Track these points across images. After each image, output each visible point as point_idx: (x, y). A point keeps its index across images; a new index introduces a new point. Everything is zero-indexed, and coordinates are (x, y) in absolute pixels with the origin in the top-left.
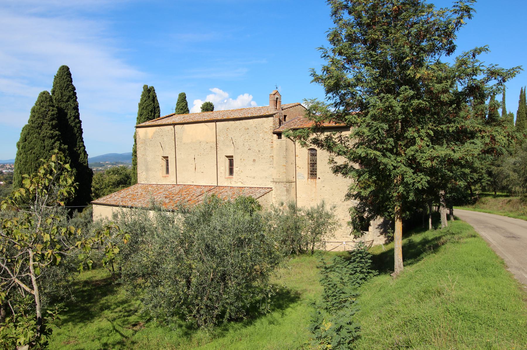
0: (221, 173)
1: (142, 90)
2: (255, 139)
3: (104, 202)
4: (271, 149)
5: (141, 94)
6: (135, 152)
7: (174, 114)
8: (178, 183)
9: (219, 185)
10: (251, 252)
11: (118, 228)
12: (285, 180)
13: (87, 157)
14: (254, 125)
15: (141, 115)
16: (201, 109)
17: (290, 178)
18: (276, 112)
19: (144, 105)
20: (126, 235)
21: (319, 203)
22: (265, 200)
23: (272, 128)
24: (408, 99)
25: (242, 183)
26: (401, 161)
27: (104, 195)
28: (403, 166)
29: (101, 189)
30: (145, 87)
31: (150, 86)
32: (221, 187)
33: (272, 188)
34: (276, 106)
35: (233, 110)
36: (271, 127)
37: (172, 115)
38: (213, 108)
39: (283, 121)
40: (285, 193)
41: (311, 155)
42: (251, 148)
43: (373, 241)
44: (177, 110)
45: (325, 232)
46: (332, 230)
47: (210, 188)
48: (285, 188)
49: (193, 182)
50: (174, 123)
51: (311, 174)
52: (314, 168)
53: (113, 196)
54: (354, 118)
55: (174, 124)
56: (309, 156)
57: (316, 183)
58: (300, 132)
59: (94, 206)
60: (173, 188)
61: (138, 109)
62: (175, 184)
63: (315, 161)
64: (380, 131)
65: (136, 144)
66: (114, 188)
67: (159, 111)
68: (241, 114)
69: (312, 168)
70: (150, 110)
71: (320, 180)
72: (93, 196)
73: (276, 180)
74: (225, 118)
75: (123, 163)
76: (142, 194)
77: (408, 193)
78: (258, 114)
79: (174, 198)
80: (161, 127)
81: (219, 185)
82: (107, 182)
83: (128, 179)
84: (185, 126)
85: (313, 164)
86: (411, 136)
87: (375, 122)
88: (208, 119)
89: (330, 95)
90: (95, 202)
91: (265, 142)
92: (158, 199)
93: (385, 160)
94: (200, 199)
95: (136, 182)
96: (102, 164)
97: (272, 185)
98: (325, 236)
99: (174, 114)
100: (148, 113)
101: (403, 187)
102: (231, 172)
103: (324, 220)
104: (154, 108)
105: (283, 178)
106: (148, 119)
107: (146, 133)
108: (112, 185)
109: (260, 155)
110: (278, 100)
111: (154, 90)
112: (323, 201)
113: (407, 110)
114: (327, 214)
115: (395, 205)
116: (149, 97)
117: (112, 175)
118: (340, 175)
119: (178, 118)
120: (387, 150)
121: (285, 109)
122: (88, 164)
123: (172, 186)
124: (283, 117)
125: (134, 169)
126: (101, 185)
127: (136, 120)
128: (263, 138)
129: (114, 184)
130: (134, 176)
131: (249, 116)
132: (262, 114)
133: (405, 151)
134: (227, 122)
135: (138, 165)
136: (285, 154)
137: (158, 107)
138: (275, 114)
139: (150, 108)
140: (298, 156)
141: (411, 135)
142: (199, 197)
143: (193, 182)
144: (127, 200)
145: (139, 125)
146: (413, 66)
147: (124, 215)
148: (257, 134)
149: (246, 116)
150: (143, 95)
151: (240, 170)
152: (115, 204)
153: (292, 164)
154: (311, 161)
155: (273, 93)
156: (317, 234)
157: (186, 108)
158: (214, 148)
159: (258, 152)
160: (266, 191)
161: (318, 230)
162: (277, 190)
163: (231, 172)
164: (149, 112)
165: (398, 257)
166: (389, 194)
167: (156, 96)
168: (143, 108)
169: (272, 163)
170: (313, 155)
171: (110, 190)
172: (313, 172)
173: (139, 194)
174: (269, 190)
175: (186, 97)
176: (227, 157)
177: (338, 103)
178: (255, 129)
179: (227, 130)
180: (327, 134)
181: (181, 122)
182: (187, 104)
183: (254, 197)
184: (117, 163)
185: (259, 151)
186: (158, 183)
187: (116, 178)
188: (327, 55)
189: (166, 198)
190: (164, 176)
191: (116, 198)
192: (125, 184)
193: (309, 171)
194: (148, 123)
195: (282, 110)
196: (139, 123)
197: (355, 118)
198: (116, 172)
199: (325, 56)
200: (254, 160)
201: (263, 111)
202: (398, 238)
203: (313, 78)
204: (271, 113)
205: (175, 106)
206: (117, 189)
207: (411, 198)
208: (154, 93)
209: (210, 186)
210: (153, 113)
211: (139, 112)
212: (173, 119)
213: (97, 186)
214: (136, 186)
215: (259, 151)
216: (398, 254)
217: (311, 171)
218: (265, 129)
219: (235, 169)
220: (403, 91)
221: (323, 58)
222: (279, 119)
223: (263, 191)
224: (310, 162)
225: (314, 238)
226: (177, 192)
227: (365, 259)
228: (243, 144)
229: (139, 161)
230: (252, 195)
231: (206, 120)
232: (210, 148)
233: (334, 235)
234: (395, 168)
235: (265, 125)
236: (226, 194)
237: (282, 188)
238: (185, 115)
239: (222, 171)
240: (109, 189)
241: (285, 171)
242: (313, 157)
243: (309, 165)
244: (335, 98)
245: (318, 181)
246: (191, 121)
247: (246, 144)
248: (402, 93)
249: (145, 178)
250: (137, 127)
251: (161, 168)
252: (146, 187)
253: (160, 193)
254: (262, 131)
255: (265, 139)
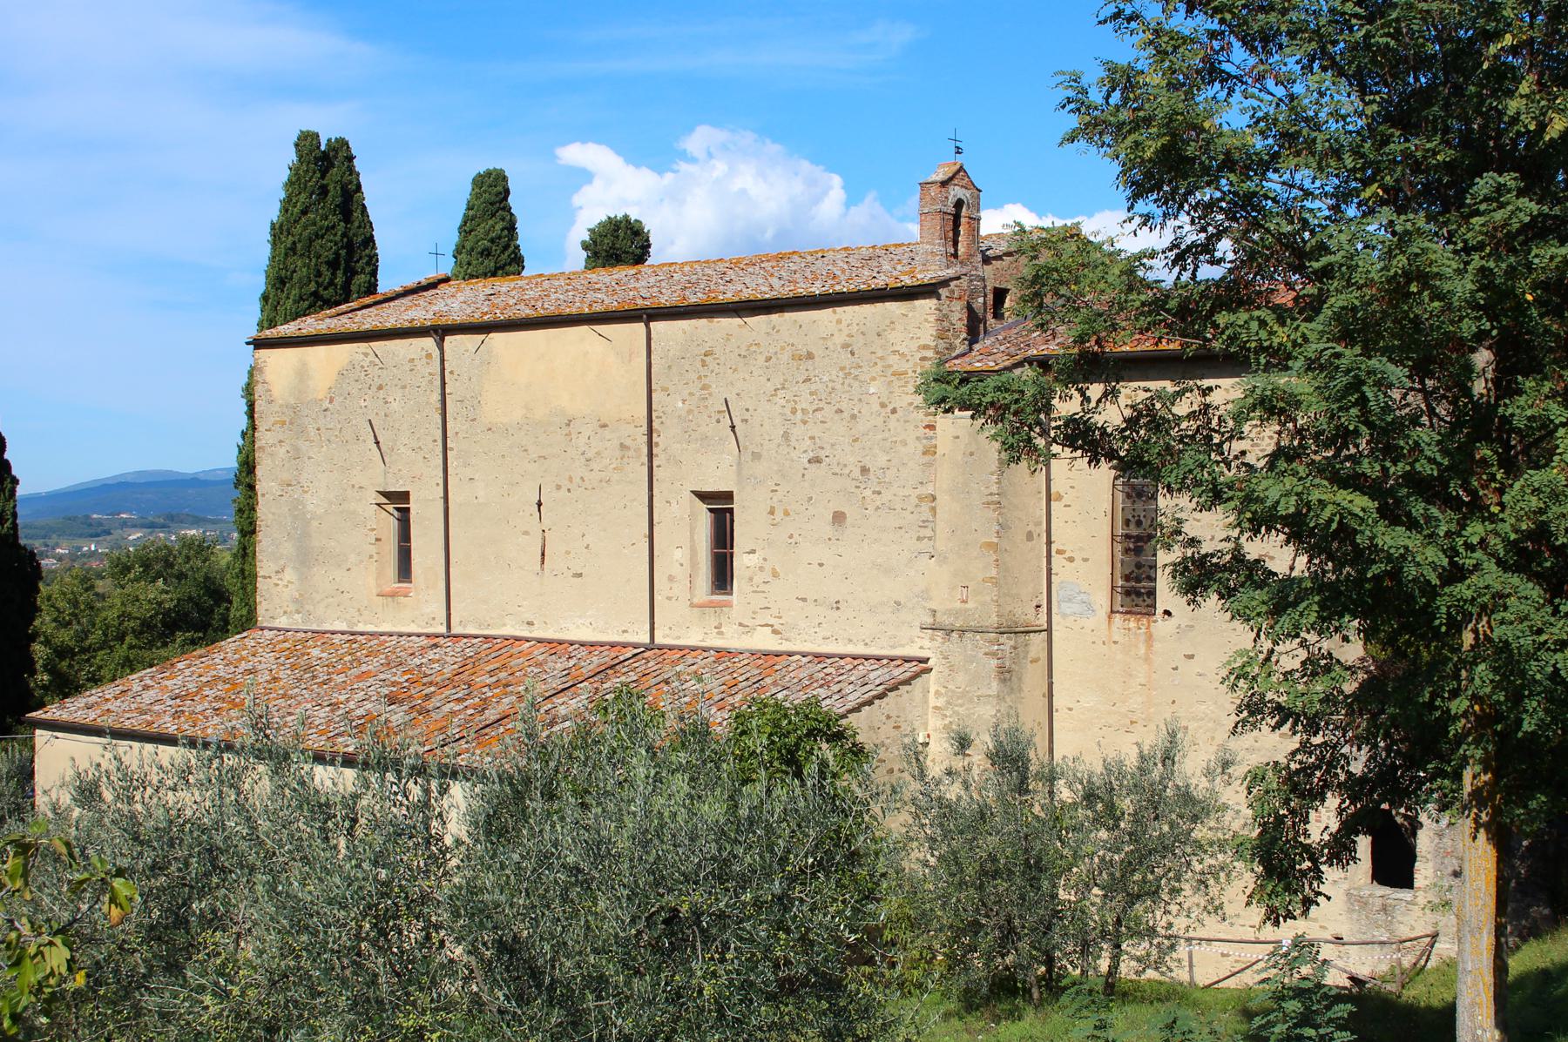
0: (671, 578)
1: (291, 156)
2: (844, 406)
3: (90, 717)
4: (927, 458)
5: (285, 175)
6: (248, 466)
7: (446, 280)
8: (456, 630)
9: (659, 640)
10: (724, 980)
11: (64, 850)
12: (993, 620)
13: (13, 492)
14: (840, 339)
15: (279, 281)
16: (584, 254)
17: (1018, 611)
18: (951, 272)
19: (298, 229)
20: (118, 883)
21: (1152, 739)
22: (891, 723)
23: (930, 354)
24: (1512, 241)
25: (775, 632)
26: (1483, 542)
27: (95, 680)
28: (1490, 566)
29: (84, 650)
30: (307, 142)
31: (327, 134)
32: (671, 648)
33: (926, 660)
34: (956, 243)
35: (738, 261)
36: (926, 347)
37: (433, 285)
38: (645, 247)
39: (989, 316)
40: (995, 684)
41: (1128, 496)
42: (822, 454)
43: (1434, 936)
44: (464, 257)
45: (1175, 892)
46: (1211, 882)
47: (616, 656)
48: (994, 662)
49: (530, 624)
50: (443, 321)
51: (1128, 593)
52: (1143, 559)
53: (136, 687)
54: (1254, 325)
55: (441, 332)
56: (1120, 496)
57: (1149, 638)
58: (998, 389)
59: (41, 736)
60: (431, 655)
61: (267, 250)
62: (443, 630)
63: (1146, 523)
64: (1370, 395)
65: (254, 429)
66: (150, 645)
67: (373, 261)
68: (775, 282)
69: (1129, 559)
70: (328, 255)
71: (1171, 623)
72: (44, 687)
73: (946, 620)
74: (693, 300)
75: (205, 520)
76: (275, 679)
77: (1516, 698)
78: (865, 280)
79: (434, 702)
80: (377, 345)
81: (659, 640)
82: (112, 615)
83: (218, 604)
84: (497, 338)
85: (1138, 538)
86: (1530, 419)
87: (1348, 352)
88: (611, 303)
89: (1142, 206)
90: (48, 716)
91: (892, 423)
92: (352, 705)
93: (1393, 539)
94: (562, 711)
95: (249, 621)
96: (100, 523)
97: (927, 643)
98: (1174, 908)
99: (446, 280)
100: (319, 274)
101: (1495, 670)
102: (722, 575)
103: (1172, 825)
104: (350, 246)
105: (983, 608)
106: (318, 302)
107: (302, 373)
108: (138, 634)
109: (868, 493)
110: (964, 211)
111: (350, 158)
112: (1173, 735)
113: (1509, 293)
114: (1186, 797)
115: (1464, 761)
116: (324, 191)
117: (137, 580)
118: (1212, 602)
119: (460, 302)
120: (1415, 482)
121: (998, 258)
122: (15, 526)
123: (425, 642)
124: (990, 297)
125: (245, 555)
126: (86, 634)
127: (257, 306)
128: (883, 405)
129: (146, 625)
130: (244, 588)
131: (817, 289)
132: (880, 282)
133: (1501, 491)
134: (702, 323)
135: (260, 536)
136: (994, 489)
137: (370, 241)
138: (945, 283)
139: (327, 248)
140: (1060, 498)
141: (1529, 413)
142: (558, 700)
143: (530, 624)
144: (199, 708)
145: (268, 333)
146: (1532, 77)
147: (130, 784)
148: (856, 384)
149: (802, 289)
150: (296, 183)
151: (768, 566)
152: (143, 728)
153: (1030, 536)
154: (1127, 523)
155: (941, 177)
156: (1133, 898)
157: (506, 247)
158: (637, 450)
159: (857, 473)
160: (896, 672)
161: (1137, 877)
162: (952, 669)
163: (722, 575)
164: (324, 268)
165: (1472, 1016)
166: (1430, 706)
167: (359, 187)
168: (293, 249)
169: (928, 533)
170: (1140, 495)
171: (127, 658)
172: (1138, 580)
173: (264, 677)
174: (913, 668)
175: (507, 192)
176: (703, 496)
177: (1189, 248)
178: (845, 356)
179: (704, 364)
180: (1133, 392)
181: (477, 318)
182: (511, 228)
183: (832, 705)
184: (172, 520)
185: (864, 470)
186: (360, 628)
187: (158, 594)
188: (1128, 11)
189: (392, 700)
190: (387, 589)
191: (149, 696)
192: (203, 626)
193: (1118, 574)
194: (311, 324)
195: (987, 260)
196: (272, 324)
197: (1263, 323)
198: (156, 565)
199: (1116, 16)
200: (839, 518)
201: (886, 267)
202: (1474, 923)
203: (1073, 121)
204: (925, 277)
205: (454, 238)
206: (163, 652)
207: (1528, 726)
208: (351, 170)
209: (613, 645)
210: (340, 273)
211: (271, 266)
212: (439, 306)
213: (65, 637)
214: (250, 638)
215: (864, 470)
216: (1473, 1004)
217: (1127, 578)
218: (893, 360)
219: (742, 562)
220: (1486, 199)
221: (1110, 26)
222: (970, 308)
223: (879, 675)
224: (1120, 531)
225: (1119, 922)
226: (448, 671)
227: (1316, 1027)
228: (786, 436)
229: (265, 511)
230: (822, 692)
231: (598, 308)
232: (618, 453)
233: (1221, 906)
234: (1455, 574)
235: (894, 337)
236: (693, 686)
237: (978, 657)
238: (503, 285)
239: (676, 570)
240: (121, 651)
241: (993, 572)
242: (1139, 505)
243: (1118, 547)
244: (1171, 223)
245: (1161, 626)
246: (526, 312)
247: (797, 431)
248: (1483, 207)
249: (296, 601)
250: (259, 344)
251: (373, 550)
252: (295, 646)
253: (363, 676)
254: (879, 368)
255: (894, 411)
